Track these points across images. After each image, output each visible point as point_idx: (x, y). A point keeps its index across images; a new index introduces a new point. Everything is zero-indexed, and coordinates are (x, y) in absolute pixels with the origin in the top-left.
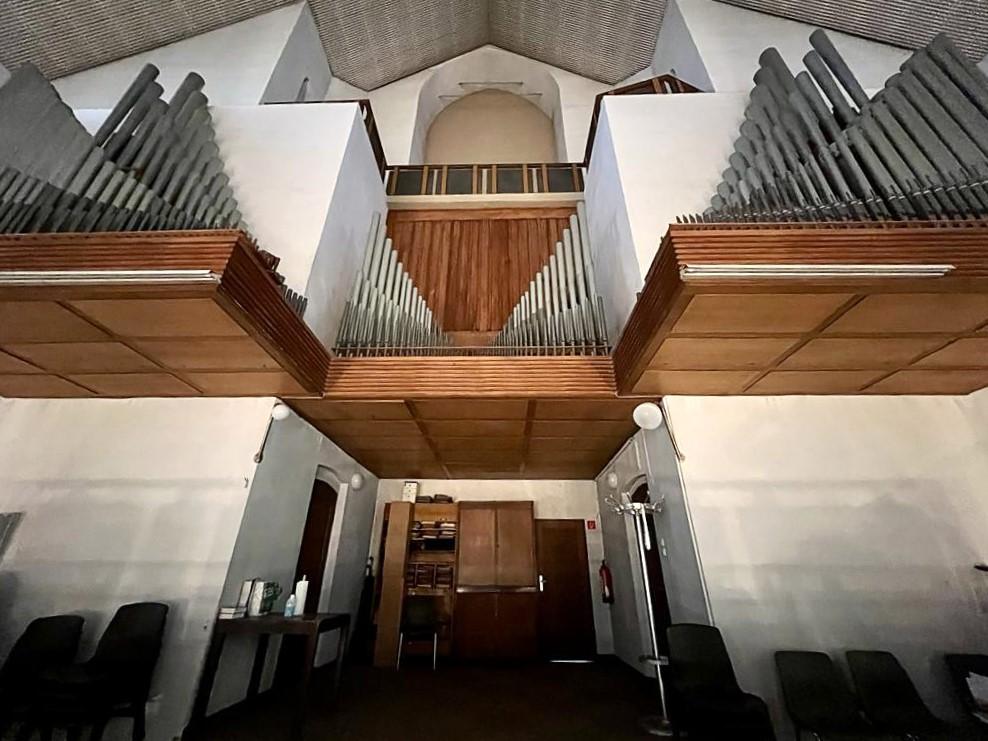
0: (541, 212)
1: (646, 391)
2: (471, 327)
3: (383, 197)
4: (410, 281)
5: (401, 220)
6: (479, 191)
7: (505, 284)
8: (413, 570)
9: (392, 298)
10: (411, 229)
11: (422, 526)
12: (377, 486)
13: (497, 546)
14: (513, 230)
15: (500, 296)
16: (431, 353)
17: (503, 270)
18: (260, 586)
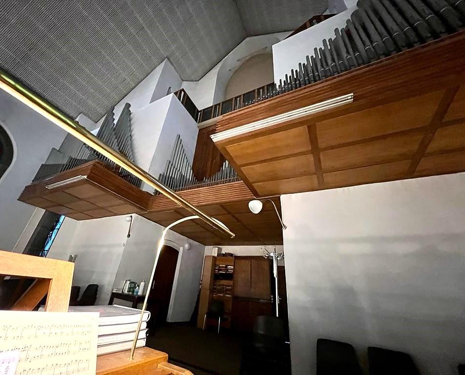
1: (268, 194)
8: (215, 287)
11: (220, 267)
12: (204, 249)
13: (251, 278)
18: (128, 282)
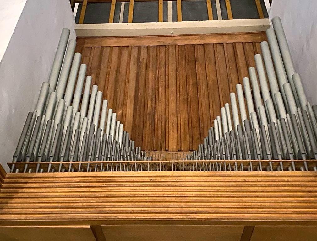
0: (226, 37)
2: (161, 147)
3: (72, 25)
4: (100, 93)
5: (89, 45)
6: (165, 20)
7: (194, 105)
9: (79, 110)
10: (99, 53)
14: (200, 53)
15: (189, 116)
16: (124, 168)
17: (191, 91)
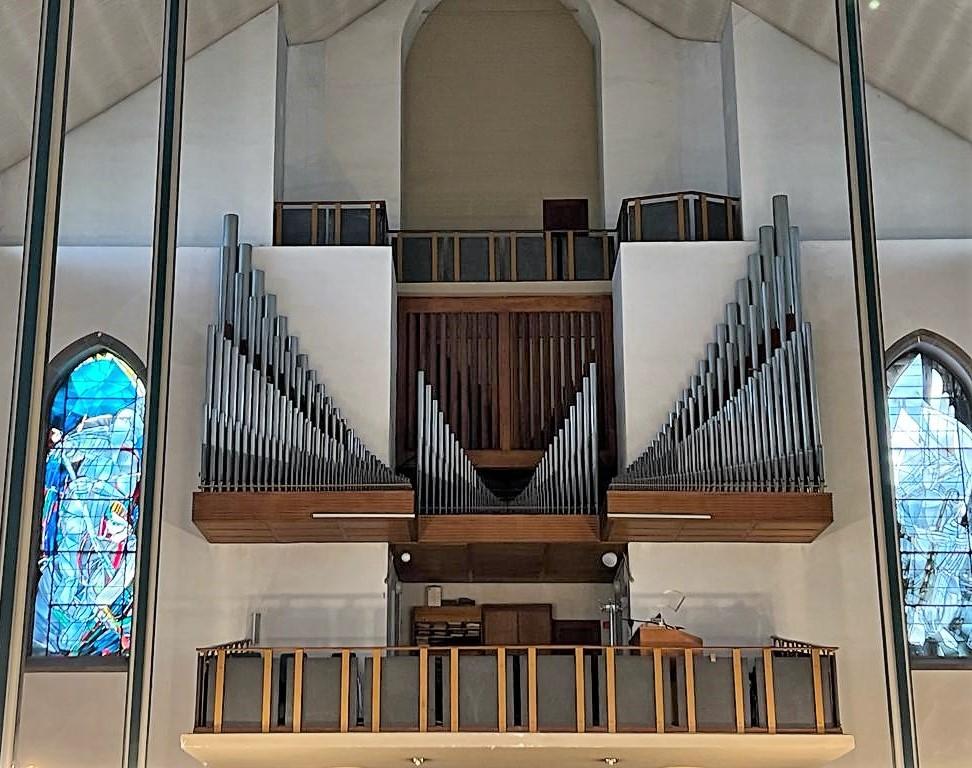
0: (565, 302)
11: (448, 626)
